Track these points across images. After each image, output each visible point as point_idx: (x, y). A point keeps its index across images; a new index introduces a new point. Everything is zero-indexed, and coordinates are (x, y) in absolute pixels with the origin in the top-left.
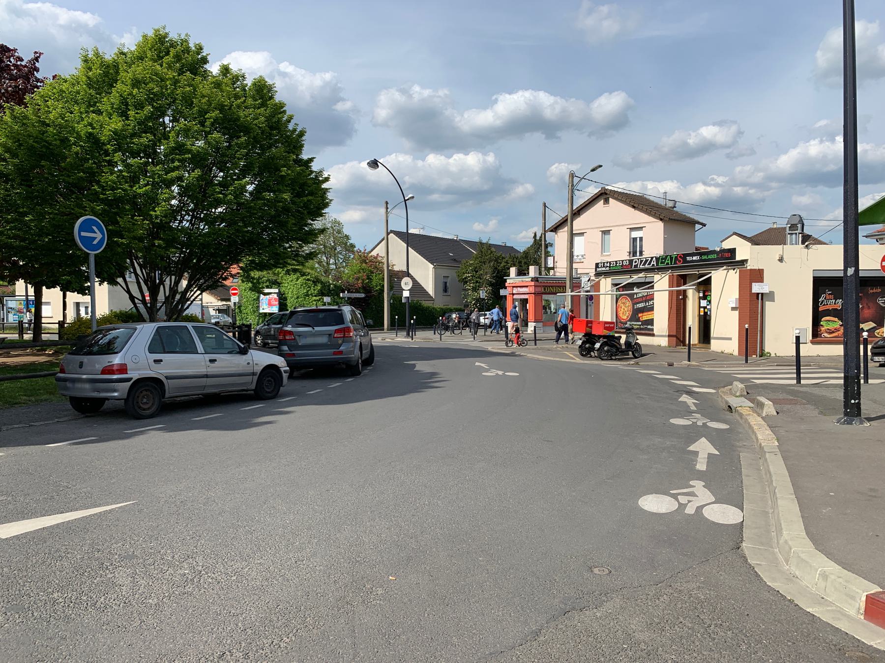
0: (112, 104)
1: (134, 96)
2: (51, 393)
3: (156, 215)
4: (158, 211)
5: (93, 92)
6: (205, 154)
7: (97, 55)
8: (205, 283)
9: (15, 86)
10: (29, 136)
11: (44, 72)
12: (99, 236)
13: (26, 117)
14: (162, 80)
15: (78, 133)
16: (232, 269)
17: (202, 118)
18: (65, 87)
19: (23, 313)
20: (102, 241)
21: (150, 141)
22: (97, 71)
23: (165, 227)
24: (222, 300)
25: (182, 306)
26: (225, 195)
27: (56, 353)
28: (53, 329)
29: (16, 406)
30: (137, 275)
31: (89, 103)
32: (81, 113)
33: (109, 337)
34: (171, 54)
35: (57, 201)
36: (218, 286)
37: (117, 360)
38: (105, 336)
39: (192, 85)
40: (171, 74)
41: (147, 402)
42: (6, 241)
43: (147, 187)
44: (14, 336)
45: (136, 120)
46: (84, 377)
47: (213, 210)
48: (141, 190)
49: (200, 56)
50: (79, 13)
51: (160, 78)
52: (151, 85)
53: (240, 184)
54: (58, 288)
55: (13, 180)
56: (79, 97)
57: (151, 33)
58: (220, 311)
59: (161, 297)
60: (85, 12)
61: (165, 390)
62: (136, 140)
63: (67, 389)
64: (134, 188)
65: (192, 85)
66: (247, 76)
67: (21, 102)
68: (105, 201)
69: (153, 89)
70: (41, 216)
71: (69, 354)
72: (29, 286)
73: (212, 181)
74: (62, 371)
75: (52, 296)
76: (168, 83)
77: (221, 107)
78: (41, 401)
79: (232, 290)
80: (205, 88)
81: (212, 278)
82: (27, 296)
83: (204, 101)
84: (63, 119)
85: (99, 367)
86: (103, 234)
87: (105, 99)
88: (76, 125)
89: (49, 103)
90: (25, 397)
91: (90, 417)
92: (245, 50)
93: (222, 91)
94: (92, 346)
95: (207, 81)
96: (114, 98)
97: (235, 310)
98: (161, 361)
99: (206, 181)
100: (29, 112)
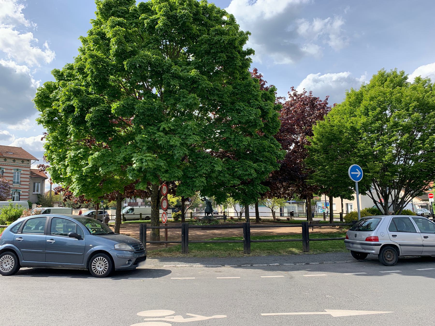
0: (361, 111)
1: (371, 105)
2: (341, 248)
3: (385, 160)
4: (387, 157)
5: (352, 108)
6: (410, 125)
7: (353, 91)
8: (414, 193)
9: (320, 113)
10: (326, 132)
11: (330, 104)
12: (359, 173)
13: (324, 125)
14: (384, 94)
15: (347, 128)
16: (430, 184)
17: (407, 107)
18: (340, 108)
19: (324, 208)
20: (361, 175)
21: (380, 124)
22: (353, 98)
23: (390, 165)
24: (423, 200)
25: (402, 205)
26: (424, 145)
27: (340, 228)
28: (337, 216)
29: (328, 252)
30: (377, 190)
31: (350, 113)
32: (347, 118)
33: (366, 223)
34: (388, 80)
35: (338, 159)
36: (423, 194)
37: (373, 234)
38: (365, 222)
39: (400, 92)
40: (389, 90)
41: (390, 257)
42: (319, 178)
43: (380, 147)
44: (322, 219)
45: (373, 116)
46: (358, 241)
47: (417, 154)
48: (377, 149)
49: (403, 77)
50: (341, 73)
51: (383, 93)
52: (379, 98)
53: (433, 137)
54: (339, 198)
55: (320, 152)
56: (346, 111)
57: (377, 73)
58: (422, 207)
59: (390, 200)
60: (343, 72)
61: (399, 252)
62: (373, 125)
63: (350, 247)
64: (374, 148)
65: (400, 92)
66: (431, 79)
67: (322, 119)
68: (361, 156)
69: (380, 99)
70: (332, 166)
71: (350, 230)
72: (326, 196)
73: (415, 138)
74: (347, 238)
75: (337, 201)
76: (387, 94)
77: (418, 100)
78: (338, 251)
79: (430, 195)
80: (407, 92)
81: (418, 189)
82: (326, 201)
83: (407, 98)
84: (340, 122)
85: (364, 237)
86: (361, 172)
87: (357, 110)
88: (346, 124)
89: (334, 117)
90: (331, 249)
91: (361, 261)
92: (425, 64)
93: (417, 91)
94: (359, 227)
95: (408, 88)
96: (362, 108)
97: (432, 206)
98: (396, 236)
99: (412, 139)
100: (325, 122)
